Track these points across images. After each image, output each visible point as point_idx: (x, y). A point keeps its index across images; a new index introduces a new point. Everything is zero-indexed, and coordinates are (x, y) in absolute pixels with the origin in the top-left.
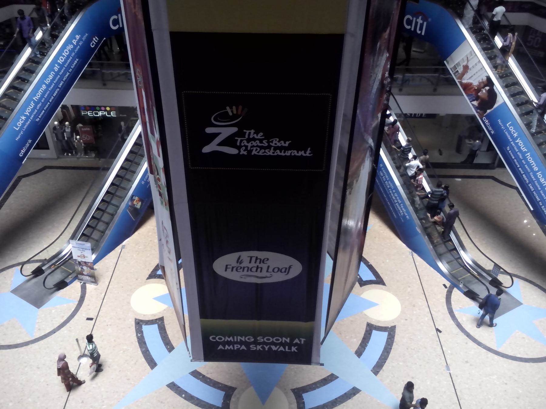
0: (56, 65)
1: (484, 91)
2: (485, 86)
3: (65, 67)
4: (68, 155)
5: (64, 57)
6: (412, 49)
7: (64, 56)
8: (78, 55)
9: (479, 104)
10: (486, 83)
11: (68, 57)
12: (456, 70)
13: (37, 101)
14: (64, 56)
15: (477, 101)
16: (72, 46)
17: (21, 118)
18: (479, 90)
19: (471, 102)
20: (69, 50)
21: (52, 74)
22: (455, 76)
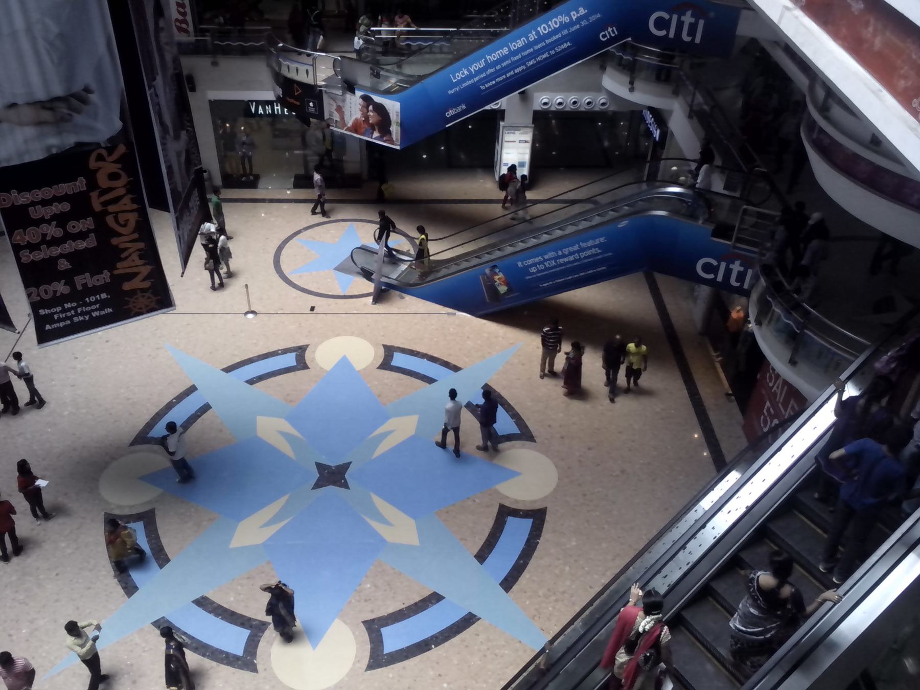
0: (534, 33)
1: (371, 114)
2: (367, 107)
3: (545, 42)
5: (549, 28)
7: (549, 27)
8: (572, 37)
9: (379, 132)
10: (365, 104)
11: (555, 32)
12: (335, 121)
13: (489, 62)
14: (549, 27)
15: (375, 130)
16: (568, 19)
17: (462, 70)
18: (367, 118)
19: (371, 138)
20: (561, 23)
21: (524, 40)
22: (338, 128)
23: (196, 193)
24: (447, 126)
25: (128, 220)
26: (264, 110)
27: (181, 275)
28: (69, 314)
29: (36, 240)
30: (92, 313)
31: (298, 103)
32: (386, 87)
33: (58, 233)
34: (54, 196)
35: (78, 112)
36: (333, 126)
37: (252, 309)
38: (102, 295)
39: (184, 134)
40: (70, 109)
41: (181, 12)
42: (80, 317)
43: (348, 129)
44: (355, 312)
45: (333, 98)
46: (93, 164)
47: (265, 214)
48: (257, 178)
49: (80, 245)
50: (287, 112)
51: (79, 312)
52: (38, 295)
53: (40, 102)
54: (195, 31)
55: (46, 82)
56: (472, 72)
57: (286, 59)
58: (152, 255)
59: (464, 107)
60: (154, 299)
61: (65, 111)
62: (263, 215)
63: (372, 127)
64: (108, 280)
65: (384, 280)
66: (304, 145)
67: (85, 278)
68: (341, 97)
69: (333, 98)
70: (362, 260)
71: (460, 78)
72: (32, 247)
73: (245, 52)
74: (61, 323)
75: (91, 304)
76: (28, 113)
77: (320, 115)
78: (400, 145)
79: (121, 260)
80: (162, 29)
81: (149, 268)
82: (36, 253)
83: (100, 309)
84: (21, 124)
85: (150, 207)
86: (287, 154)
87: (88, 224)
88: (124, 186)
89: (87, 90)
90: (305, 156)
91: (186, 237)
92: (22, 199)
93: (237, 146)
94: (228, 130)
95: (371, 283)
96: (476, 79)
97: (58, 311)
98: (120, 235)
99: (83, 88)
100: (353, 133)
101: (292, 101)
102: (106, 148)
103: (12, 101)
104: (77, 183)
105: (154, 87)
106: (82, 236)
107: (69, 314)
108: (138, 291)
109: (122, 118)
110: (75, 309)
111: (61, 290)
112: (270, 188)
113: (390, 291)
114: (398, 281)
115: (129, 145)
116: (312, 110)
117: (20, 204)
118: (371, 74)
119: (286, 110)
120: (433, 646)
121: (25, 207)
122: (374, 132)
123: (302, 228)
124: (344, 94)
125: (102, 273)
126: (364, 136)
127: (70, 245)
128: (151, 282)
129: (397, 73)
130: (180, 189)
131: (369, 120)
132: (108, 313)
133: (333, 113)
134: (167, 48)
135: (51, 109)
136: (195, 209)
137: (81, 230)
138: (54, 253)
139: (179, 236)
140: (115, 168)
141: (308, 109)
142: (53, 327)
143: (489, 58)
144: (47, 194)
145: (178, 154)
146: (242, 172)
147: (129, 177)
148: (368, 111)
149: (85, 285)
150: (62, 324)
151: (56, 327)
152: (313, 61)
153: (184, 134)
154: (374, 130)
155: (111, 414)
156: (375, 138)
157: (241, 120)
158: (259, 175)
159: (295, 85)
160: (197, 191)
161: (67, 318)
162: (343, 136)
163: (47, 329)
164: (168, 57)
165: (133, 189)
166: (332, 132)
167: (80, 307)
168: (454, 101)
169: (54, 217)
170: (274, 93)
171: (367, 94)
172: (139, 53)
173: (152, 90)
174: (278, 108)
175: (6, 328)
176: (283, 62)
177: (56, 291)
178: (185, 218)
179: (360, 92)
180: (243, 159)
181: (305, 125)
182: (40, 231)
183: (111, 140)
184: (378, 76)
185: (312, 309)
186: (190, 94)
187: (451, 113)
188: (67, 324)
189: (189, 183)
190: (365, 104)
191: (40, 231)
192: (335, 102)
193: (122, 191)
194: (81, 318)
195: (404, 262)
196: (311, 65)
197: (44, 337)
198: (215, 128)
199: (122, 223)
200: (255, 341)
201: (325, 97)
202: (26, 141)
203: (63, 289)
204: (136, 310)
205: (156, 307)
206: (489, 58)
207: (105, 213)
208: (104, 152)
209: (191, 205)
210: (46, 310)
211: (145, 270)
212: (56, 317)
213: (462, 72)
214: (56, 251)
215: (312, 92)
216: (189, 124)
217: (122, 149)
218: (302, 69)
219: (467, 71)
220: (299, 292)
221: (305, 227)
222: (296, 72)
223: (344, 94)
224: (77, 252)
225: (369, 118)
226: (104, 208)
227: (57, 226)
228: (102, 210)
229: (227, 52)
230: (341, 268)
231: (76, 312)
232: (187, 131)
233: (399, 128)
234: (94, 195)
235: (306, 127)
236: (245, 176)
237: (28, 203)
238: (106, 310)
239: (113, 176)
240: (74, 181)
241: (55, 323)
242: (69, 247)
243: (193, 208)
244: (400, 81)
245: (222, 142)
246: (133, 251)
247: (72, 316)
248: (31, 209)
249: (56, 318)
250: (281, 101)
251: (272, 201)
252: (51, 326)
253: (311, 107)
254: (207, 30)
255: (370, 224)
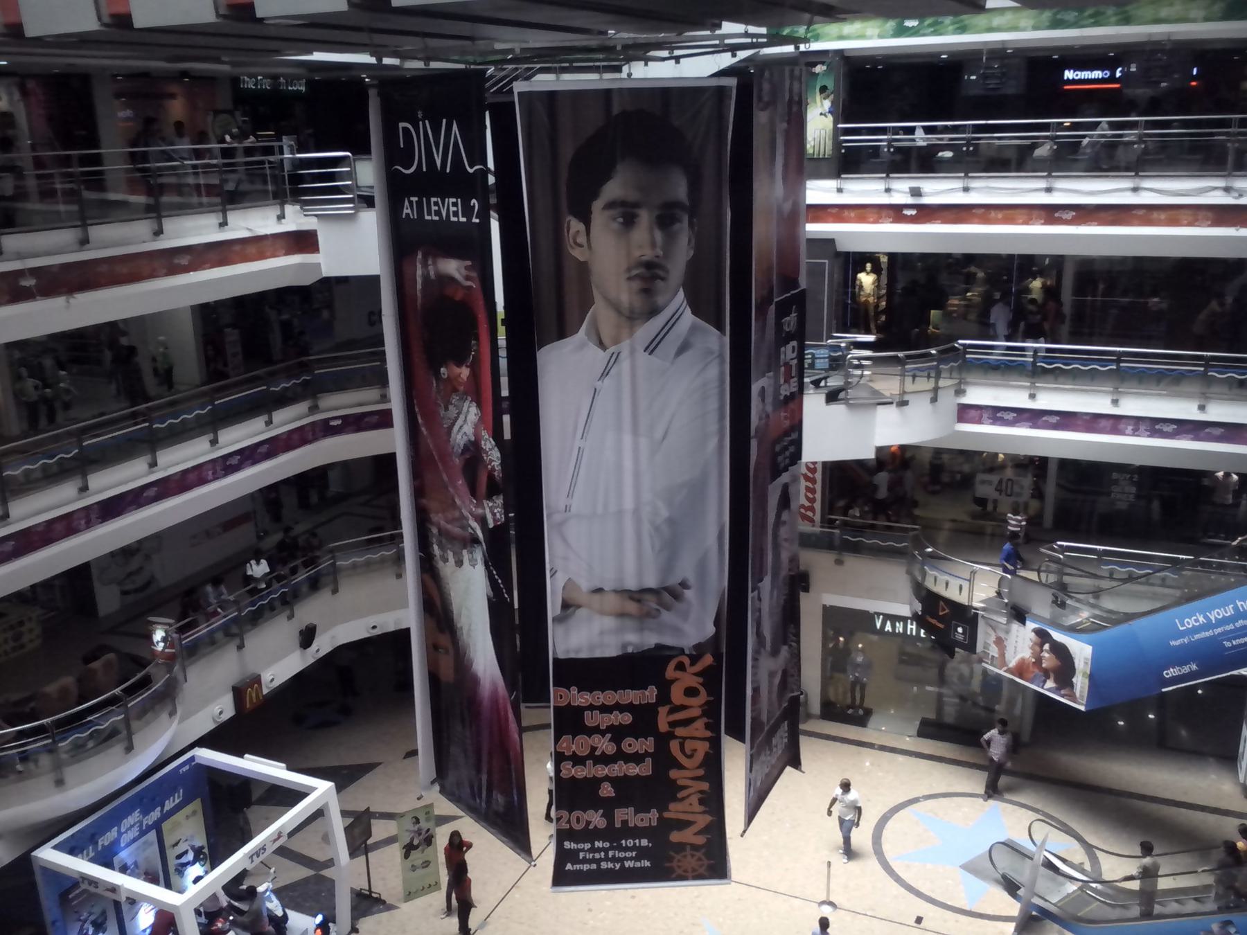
1: (1046, 655)
2: (1041, 646)
4: (1227, 475)
6: (970, 267)
9: (1056, 681)
12: (990, 657)
15: (1049, 678)
17: (1196, 616)
18: (1039, 661)
19: (1042, 688)
23: (785, 726)
24: (1164, 690)
25: (695, 750)
26: (893, 626)
28: (597, 856)
30: (625, 862)
31: (941, 626)
32: (1073, 622)
34: (617, 703)
35: (668, 608)
36: (987, 663)
42: (609, 863)
43: (1009, 671)
45: (993, 626)
46: (670, 672)
48: (868, 713)
50: (924, 634)
51: (610, 856)
54: (822, 522)
55: (640, 572)
56: (1211, 620)
58: (714, 802)
59: (1194, 667)
60: (706, 862)
61: (655, 606)
63: (1046, 674)
64: (654, 824)
65: (1036, 901)
69: (993, 626)
70: (1005, 863)
71: (1190, 626)
72: (577, 760)
75: (627, 849)
76: (612, 601)
77: (970, 646)
78: (1086, 706)
79: (675, 799)
80: (785, 523)
81: (708, 818)
83: (637, 859)
84: (602, 613)
85: (726, 733)
88: (700, 707)
89: (684, 585)
90: (940, 696)
91: (758, 784)
92: (580, 700)
93: (849, 668)
94: (841, 645)
96: (1219, 630)
97: (586, 849)
100: (1015, 676)
101: (934, 621)
102: (690, 656)
103: (599, 586)
104: (647, 693)
105: (758, 589)
106: (637, 758)
107: (597, 856)
108: (688, 848)
109: (717, 623)
110: (606, 850)
112: (883, 728)
113: (1044, 922)
114: (1058, 907)
115: (717, 656)
116: (960, 638)
118: (1053, 602)
119: (922, 631)
120: (1035, 479)
121: (580, 710)
122: (1048, 681)
123: (921, 796)
124: (1008, 622)
125: (649, 812)
126: (1032, 683)
127: (620, 767)
129: (1093, 606)
130: (764, 717)
131: (1042, 664)
133: (990, 645)
135: (639, 601)
136: (779, 747)
138: (600, 773)
139: (750, 780)
140: (694, 682)
141: (954, 636)
142: (575, 868)
143: (1242, 605)
144: (610, 696)
145: (772, 675)
146: (849, 701)
148: (1042, 651)
149: (625, 823)
150: (586, 867)
151: (578, 869)
153: (784, 651)
154: (1048, 677)
156: (1048, 688)
158: (872, 709)
160: (788, 724)
161: (593, 861)
162: (999, 678)
163: (567, 868)
165: (711, 711)
167: (613, 850)
168: (1180, 657)
169: (611, 728)
170: (910, 608)
171: (1044, 628)
172: (750, 554)
173: (756, 592)
174: (912, 627)
177: (591, 822)
179: (1033, 624)
180: (856, 682)
181: (946, 655)
184: (1063, 605)
185: (919, 920)
187: (1171, 672)
189: (778, 713)
190: (1039, 640)
191: (590, 742)
192: (995, 631)
193: (696, 712)
194: (610, 865)
195: (1072, 881)
197: (561, 878)
199: (688, 752)
202: (602, 633)
204: (680, 871)
205: (706, 873)
206: (1242, 605)
207: (671, 736)
208: (687, 661)
209: (774, 741)
210: (572, 843)
211: (703, 820)
212: (581, 855)
213: (1195, 618)
214: (602, 771)
215: (964, 615)
216: (794, 638)
217: (708, 660)
218: (954, 583)
219: (1204, 618)
220: (902, 890)
221: (925, 794)
222: (944, 585)
223: (1008, 622)
227: (611, 740)
229: (856, 549)
230: (970, 868)
232: (791, 646)
233: (1087, 681)
234: (663, 711)
235: (947, 656)
236: (852, 708)
238: (642, 861)
239: (691, 692)
241: (579, 864)
242: (618, 769)
243: (776, 746)
244: (1095, 617)
245: (830, 659)
247: (600, 860)
249: (581, 858)
250: (919, 619)
251: (883, 748)
252: (573, 866)
253: (960, 633)
255: (1024, 810)
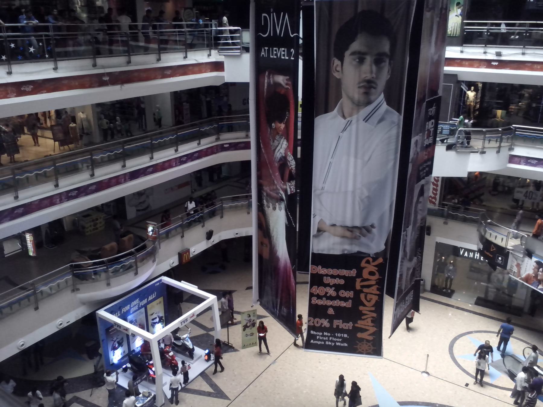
2: (539, 269)
12: (513, 272)
19: (537, 288)
23: (412, 292)
25: (372, 299)
26: (468, 254)
27: (388, 337)
28: (325, 338)
29: (322, 294)
30: (336, 343)
33: (334, 294)
36: (511, 275)
37: (427, 371)
38: (345, 335)
39: (415, 260)
40: (361, 233)
41: (434, 193)
42: (329, 342)
43: (521, 279)
44: (497, 398)
45: (516, 258)
46: (363, 264)
47: (452, 315)
48: (453, 292)
49: (342, 304)
50: (483, 259)
51: (330, 339)
52: (313, 323)
53: (347, 227)
55: (353, 219)
57: (491, 229)
58: (378, 322)
60: (372, 348)
61: (358, 234)
62: (450, 314)
66: (489, 280)
67: (339, 323)
68: (522, 259)
69: (516, 258)
72: (319, 297)
73: (465, 220)
74: (319, 342)
75: (338, 337)
76: (339, 231)
77: (504, 266)
79: (361, 319)
81: (375, 329)
82: (319, 300)
83: (342, 342)
84: (335, 235)
85: (386, 294)
86: (476, 283)
87: (350, 294)
90: (487, 287)
92: (322, 271)
94: (443, 261)
95: (513, 382)
98: (364, 305)
99: (371, 224)
101: (488, 253)
104: (352, 272)
105: (406, 231)
106: (345, 299)
107: (325, 338)
108: (365, 340)
109: (386, 244)
110: (329, 337)
111: (325, 324)
112: (459, 300)
115: (385, 259)
116: (500, 262)
117: (320, 273)
121: (322, 276)
123: (473, 331)
124: (524, 257)
125: (349, 323)
128: (373, 337)
130: (403, 288)
131: (538, 277)
132: (345, 346)
134: (420, 212)
135: (351, 231)
137: (345, 297)
139: (395, 315)
140: (374, 269)
145: (408, 269)
146: (444, 286)
147: (380, 276)
150: (319, 343)
152: (508, 234)
153: (415, 260)
155: (327, 403)
157: (452, 257)
159: (492, 245)
162: (516, 282)
164: (419, 217)
165: (380, 283)
166: (510, 278)
169: (335, 285)
170: (478, 246)
171: (541, 261)
173: (405, 232)
174: (477, 255)
175: (293, 335)
176: (488, 231)
177: (323, 324)
178: (401, 305)
182: (325, 290)
183: (377, 254)
186: (426, 236)
188: (322, 343)
189: (409, 286)
192: (517, 261)
193: (373, 282)
194: (330, 343)
196: (506, 236)
198: (436, 257)
200: (423, 392)
201: (510, 257)
202: (334, 244)
203: (326, 324)
204: (360, 350)
207: (361, 291)
208: (371, 260)
209: (407, 298)
211: (373, 330)
212: (318, 337)
214: (329, 303)
215: (503, 252)
217: (381, 260)
223: (524, 257)
224: (340, 307)
225: (538, 275)
226: (361, 289)
228: (360, 289)
229: (455, 218)
231: (329, 339)
234: (358, 280)
236: (446, 289)
237: (325, 274)
238: (344, 344)
239: (372, 273)
240: (350, 270)
242: (337, 303)
243: (407, 301)
245: (437, 266)
246: (369, 317)
248: (325, 278)
249: (317, 338)
251: (458, 308)
252: (314, 341)
253: (500, 260)
254: (447, 205)
255: (522, 342)
